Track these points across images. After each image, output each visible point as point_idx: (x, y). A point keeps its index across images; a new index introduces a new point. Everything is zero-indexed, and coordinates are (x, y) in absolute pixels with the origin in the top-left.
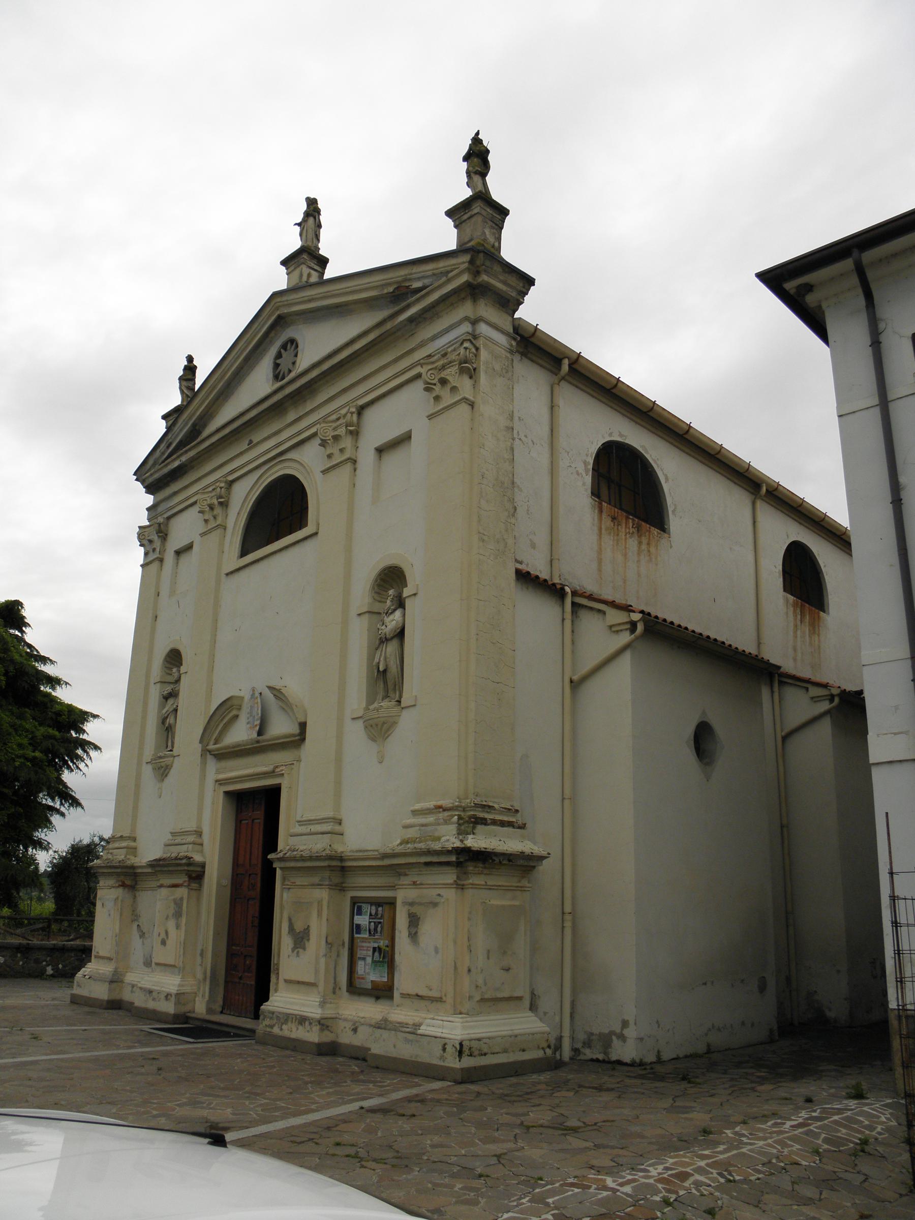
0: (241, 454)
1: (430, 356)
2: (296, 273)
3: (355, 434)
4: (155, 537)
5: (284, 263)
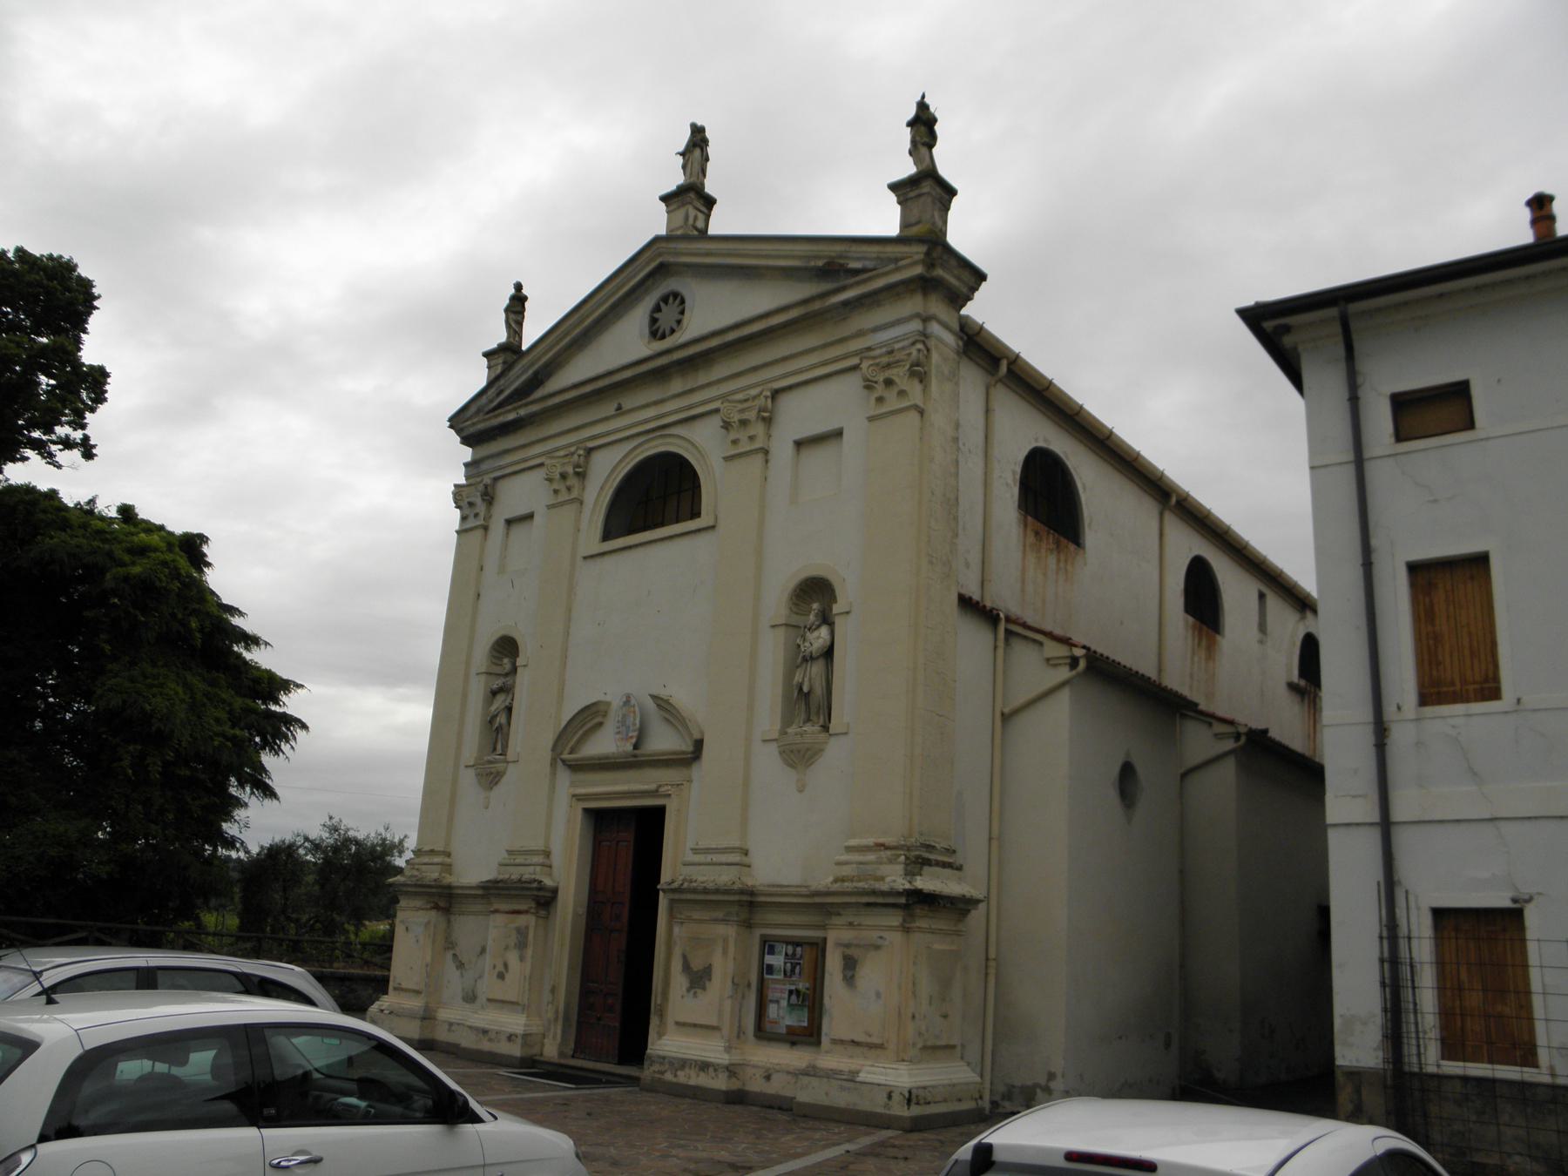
0: (606, 419)
1: (869, 349)
2: (680, 213)
3: (768, 421)
4: (478, 501)
5: (666, 199)
